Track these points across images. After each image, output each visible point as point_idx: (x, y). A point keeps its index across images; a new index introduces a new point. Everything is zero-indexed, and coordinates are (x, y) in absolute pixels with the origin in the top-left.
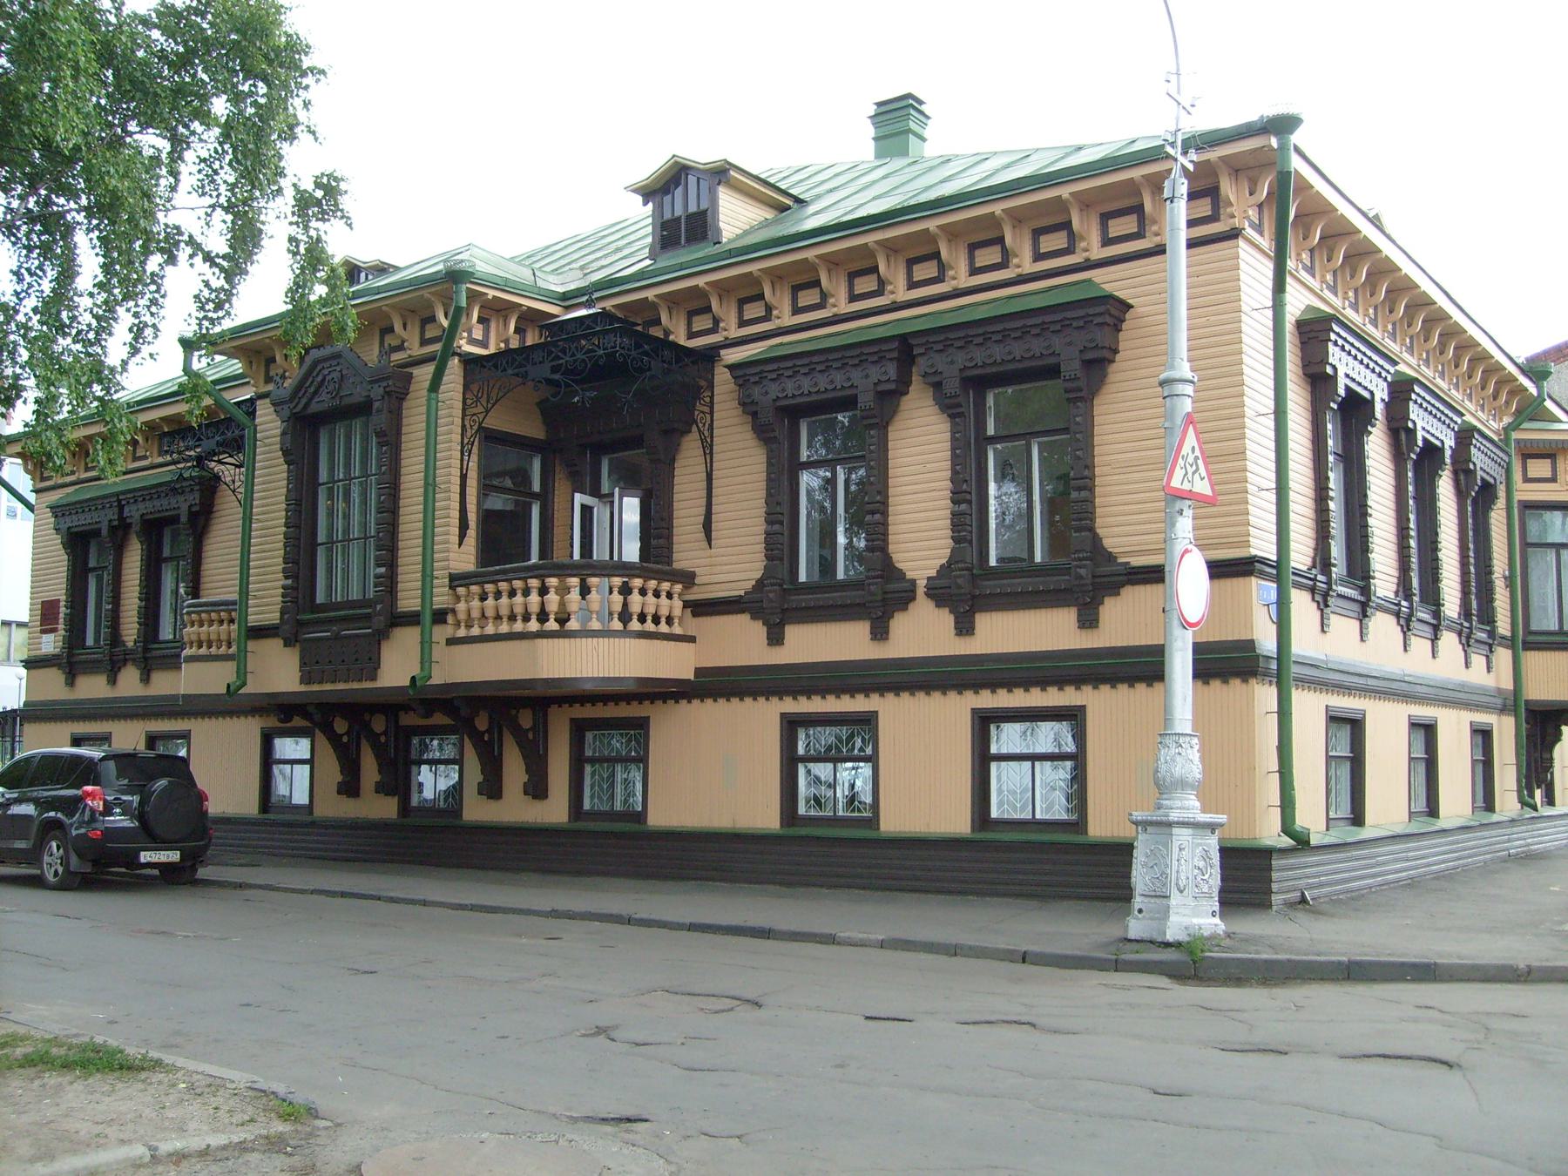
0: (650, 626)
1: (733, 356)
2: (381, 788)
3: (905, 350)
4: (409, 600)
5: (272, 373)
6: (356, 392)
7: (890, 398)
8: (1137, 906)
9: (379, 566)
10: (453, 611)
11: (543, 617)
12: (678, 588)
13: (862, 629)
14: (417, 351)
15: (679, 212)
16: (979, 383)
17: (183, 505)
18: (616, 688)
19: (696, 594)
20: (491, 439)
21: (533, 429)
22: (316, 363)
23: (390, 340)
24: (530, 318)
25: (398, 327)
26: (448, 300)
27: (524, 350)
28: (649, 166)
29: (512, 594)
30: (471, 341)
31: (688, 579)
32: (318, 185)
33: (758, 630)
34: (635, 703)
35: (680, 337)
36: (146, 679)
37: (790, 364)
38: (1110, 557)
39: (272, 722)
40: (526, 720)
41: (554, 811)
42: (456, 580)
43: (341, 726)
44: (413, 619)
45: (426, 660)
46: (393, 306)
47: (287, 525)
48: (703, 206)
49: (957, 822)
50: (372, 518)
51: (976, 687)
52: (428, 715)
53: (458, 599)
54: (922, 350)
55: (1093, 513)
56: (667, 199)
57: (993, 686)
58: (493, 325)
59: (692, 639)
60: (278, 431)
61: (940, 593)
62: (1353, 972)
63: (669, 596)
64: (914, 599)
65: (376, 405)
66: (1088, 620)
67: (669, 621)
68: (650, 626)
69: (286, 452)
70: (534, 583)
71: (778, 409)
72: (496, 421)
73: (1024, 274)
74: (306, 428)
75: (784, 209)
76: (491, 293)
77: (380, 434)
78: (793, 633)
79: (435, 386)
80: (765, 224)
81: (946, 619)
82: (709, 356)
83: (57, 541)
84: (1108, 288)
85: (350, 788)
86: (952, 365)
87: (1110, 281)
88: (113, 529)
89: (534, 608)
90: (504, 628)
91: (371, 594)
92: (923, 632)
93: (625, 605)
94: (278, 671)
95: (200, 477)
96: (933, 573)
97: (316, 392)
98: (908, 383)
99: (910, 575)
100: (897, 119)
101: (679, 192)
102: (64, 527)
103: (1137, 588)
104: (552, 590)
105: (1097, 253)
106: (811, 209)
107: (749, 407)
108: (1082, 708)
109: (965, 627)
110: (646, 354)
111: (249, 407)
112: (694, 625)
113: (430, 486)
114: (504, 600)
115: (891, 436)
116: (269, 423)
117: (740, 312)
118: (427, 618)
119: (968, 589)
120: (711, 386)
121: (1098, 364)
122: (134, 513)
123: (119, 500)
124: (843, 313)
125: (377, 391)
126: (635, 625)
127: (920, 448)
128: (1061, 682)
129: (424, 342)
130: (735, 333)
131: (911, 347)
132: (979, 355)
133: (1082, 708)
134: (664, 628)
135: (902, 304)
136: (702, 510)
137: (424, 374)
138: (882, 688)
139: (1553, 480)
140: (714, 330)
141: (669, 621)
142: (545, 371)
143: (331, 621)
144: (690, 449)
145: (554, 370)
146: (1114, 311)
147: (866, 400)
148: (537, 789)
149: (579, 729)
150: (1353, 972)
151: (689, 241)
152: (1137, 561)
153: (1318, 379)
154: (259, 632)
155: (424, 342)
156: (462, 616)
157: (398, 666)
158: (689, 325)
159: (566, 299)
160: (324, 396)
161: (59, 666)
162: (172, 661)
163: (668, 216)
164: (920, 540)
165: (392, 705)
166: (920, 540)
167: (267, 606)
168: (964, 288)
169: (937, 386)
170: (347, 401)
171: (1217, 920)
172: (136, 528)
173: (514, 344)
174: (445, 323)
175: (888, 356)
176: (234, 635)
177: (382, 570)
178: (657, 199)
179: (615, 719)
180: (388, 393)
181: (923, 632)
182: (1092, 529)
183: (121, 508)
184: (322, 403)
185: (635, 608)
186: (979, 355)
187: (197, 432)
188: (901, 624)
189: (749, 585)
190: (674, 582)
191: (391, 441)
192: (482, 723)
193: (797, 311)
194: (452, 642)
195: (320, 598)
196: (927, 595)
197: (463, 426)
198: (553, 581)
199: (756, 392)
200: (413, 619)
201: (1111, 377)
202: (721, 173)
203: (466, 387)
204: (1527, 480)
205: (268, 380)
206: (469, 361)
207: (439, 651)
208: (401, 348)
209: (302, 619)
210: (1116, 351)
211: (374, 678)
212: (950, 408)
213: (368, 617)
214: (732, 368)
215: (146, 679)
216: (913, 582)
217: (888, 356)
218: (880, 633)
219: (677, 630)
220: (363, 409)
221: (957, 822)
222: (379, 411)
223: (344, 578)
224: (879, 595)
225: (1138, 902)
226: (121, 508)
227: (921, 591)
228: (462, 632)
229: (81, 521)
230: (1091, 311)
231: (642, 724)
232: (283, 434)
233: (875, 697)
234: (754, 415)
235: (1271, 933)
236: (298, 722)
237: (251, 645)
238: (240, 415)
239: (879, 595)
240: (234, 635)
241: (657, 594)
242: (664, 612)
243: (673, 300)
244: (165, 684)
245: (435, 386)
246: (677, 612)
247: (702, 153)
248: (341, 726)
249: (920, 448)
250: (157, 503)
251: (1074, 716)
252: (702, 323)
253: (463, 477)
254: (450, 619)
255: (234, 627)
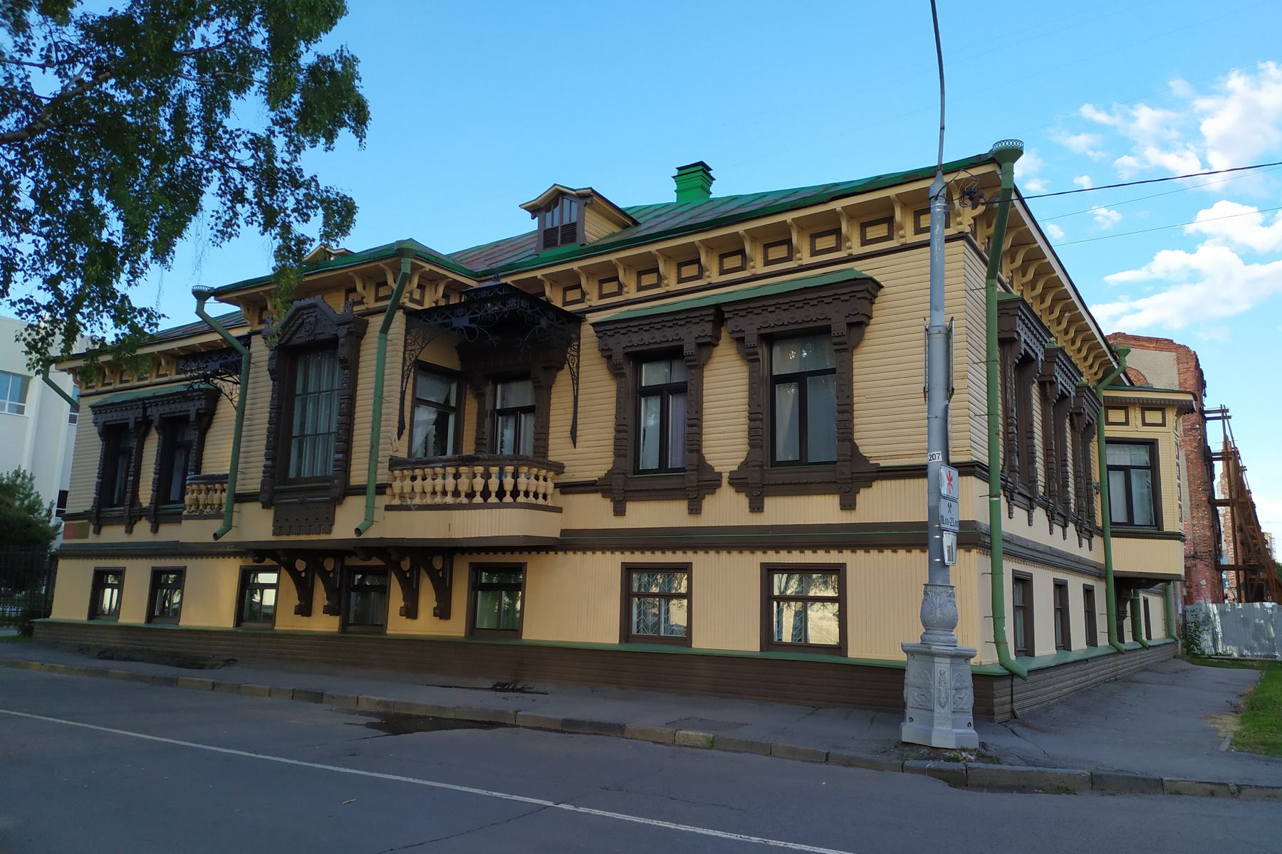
0: (531, 499)
1: (593, 318)
2: (328, 610)
3: (718, 314)
4: (358, 475)
5: (264, 317)
6: (326, 332)
7: (708, 345)
8: (908, 716)
9: (338, 453)
10: (391, 486)
11: (456, 493)
12: (551, 474)
13: (682, 506)
14: (371, 304)
15: (556, 224)
16: (770, 339)
17: (192, 408)
18: (501, 544)
19: (564, 479)
20: (423, 368)
21: (453, 363)
22: (298, 310)
23: (352, 297)
24: (452, 287)
25: (359, 287)
26: (396, 270)
27: (448, 307)
28: (536, 191)
29: (414, 478)
30: (412, 300)
31: (559, 468)
32: (309, 216)
33: (607, 505)
34: (491, 554)
35: (558, 303)
36: (155, 530)
37: (636, 323)
38: (865, 460)
39: (249, 562)
40: (438, 563)
41: (455, 627)
42: (395, 463)
43: (300, 565)
44: (360, 491)
45: (370, 520)
46: (355, 272)
47: (270, 423)
48: (574, 220)
49: (749, 643)
50: (335, 417)
51: (765, 548)
52: (369, 559)
53: (395, 479)
54: (730, 315)
55: (852, 429)
56: (549, 215)
57: (777, 548)
58: (427, 290)
59: (559, 510)
60: (267, 358)
61: (738, 482)
62: (1098, 782)
63: (545, 480)
64: (720, 486)
65: (341, 341)
66: (695, 510)
67: (545, 497)
68: (531, 499)
69: (272, 372)
70: (451, 470)
71: (627, 354)
72: (428, 356)
73: (808, 264)
74: (290, 357)
75: (625, 227)
76: (428, 267)
77: (343, 361)
78: (631, 507)
79: (385, 329)
80: (613, 234)
81: (742, 501)
82: (578, 318)
83: (94, 431)
84: (868, 274)
85: (304, 609)
86: (751, 326)
87: (864, 268)
88: (136, 423)
89: (450, 488)
90: (428, 500)
91: (330, 472)
92: (727, 509)
93: (515, 485)
94: (257, 525)
95: (207, 390)
96: (735, 468)
97: (296, 331)
98: (718, 339)
99: (717, 469)
100: (696, 175)
101: (557, 210)
102: (101, 421)
103: (884, 482)
104: (463, 476)
105: (857, 249)
106: (643, 227)
107: (606, 353)
108: (844, 565)
109: (756, 507)
110: (536, 312)
111: (246, 340)
112: (556, 499)
113: (379, 398)
114: (429, 481)
115: (706, 374)
116: (260, 351)
117: (600, 289)
118: (371, 490)
119: (758, 481)
120: (579, 339)
121: (859, 325)
122: (154, 412)
123: (144, 403)
124: (674, 291)
125: (342, 331)
126: (521, 499)
127: (726, 385)
128: (827, 547)
129: (378, 299)
130: (596, 302)
131: (723, 313)
132: (636, 339)
133: (844, 565)
134: (541, 501)
135: (717, 283)
136: (570, 422)
137: (376, 322)
138: (695, 548)
139: (1127, 423)
140: (581, 301)
141: (545, 497)
142: (463, 322)
143: (300, 490)
144: (563, 378)
145: (471, 321)
146: (871, 288)
147: (689, 349)
148: (443, 612)
149: (476, 569)
150: (1098, 782)
151: (564, 242)
152: (883, 463)
153: (1007, 342)
154: (242, 498)
155: (378, 299)
156: (397, 490)
157: (347, 522)
158: (639, 281)
159: (476, 276)
160: (302, 333)
161: (90, 519)
162: (176, 518)
163: (549, 226)
164: (726, 443)
165: (340, 551)
166: (726, 443)
167: (252, 480)
168: (762, 274)
169: (740, 341)
170: (319, 337)
171: (972, 731)
172: (156, 423)
173: (442, 303)
174: (395, 287)
175: (707, 319)
176: (224, 501)
177: (340, 456)
178: (541, 215)
179: (501, 568)
180: (350, 333)
181: (727, 509)
182: (851, 440)
183: (145, 409)
184: (301, 337)
185: (522, 487)
186: (636, 339)
187: (209, 355)
188: (709, 503)
189: (602, 474)
190: (549, 470)
191: (351, 366)
192: (406, 565)
193: (640, 289)
194: (389, 508)
195: (292, 474)
196: (730, 484)
197: (404, 359)
198: (463, 469)
199: (611, 342)
200: (360, 491)
201: (867, 336)
202: (589, 198)
203: (407, 332)
204: (1144, 424)
205: (261, 322)
206: (410, 314)
207: (379, 513)
208: (361, 303)
209: (279, 489)
210: (870, 318)
211: (329, 532)
212: (750, 357)
213: (326, 489)
214: (594, 325)
215: (155, 530)
216: (720, 474)
217: (707, 319)
218: (848, 504)
219: (550, 503)
220: (330, 345)
221: (749, 643)
222: (343, 345)
223: (311, 463)
224: (695, 483)
225: (909, 712)
226: (145, 409)
227: (725, 481)
228: (396, 502)
229: (113, 417)
230: (855, 289)
231: (520, 568)
232: (271, 359)
233: (690, 553)
234: (609, 358)
235: (1017, 746)
236: (268, 562)
237: (236, 507)
238: (238, 345)
239: (695, 483)
240: (224, 501)
241: (537, 478)
242: (541, 491)
243: (554, 279)
244: (169, 533)
245: (385, 329)
246: (550, 490)
247: (576, 182)
248: (300, 565)
249: (726, 385)
250: (173, 406)
251: (838, 570)
252: (573, 295)
253: (403, 393)
254: (388, 491)
255: (224, 494)
